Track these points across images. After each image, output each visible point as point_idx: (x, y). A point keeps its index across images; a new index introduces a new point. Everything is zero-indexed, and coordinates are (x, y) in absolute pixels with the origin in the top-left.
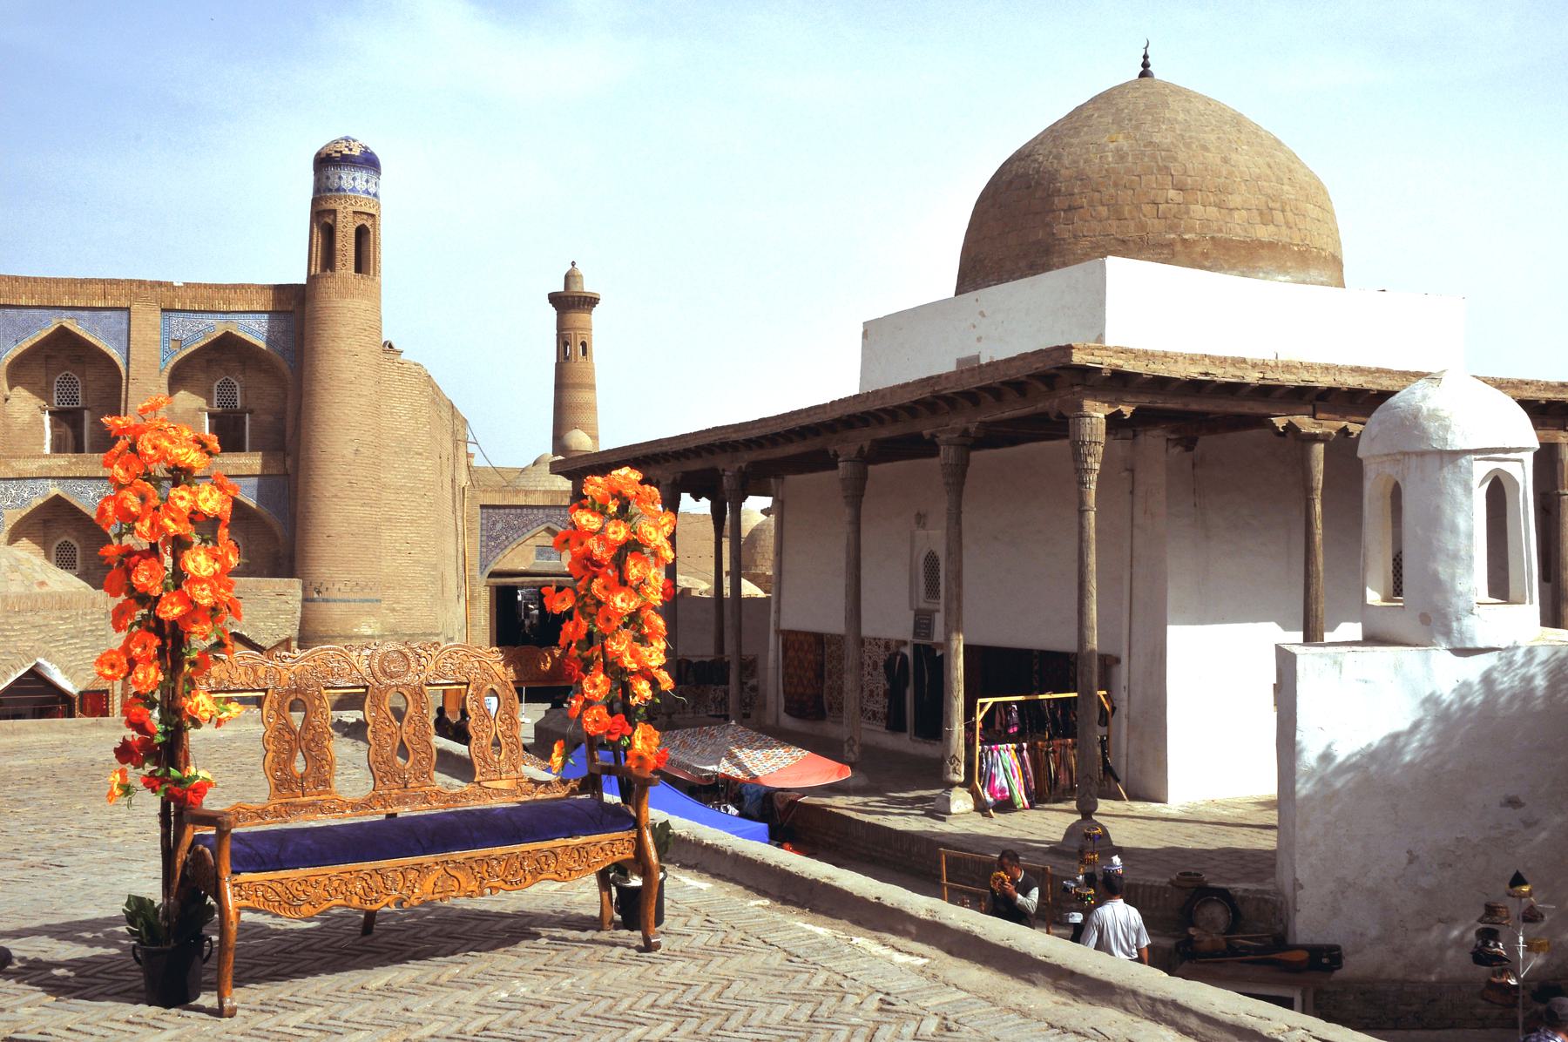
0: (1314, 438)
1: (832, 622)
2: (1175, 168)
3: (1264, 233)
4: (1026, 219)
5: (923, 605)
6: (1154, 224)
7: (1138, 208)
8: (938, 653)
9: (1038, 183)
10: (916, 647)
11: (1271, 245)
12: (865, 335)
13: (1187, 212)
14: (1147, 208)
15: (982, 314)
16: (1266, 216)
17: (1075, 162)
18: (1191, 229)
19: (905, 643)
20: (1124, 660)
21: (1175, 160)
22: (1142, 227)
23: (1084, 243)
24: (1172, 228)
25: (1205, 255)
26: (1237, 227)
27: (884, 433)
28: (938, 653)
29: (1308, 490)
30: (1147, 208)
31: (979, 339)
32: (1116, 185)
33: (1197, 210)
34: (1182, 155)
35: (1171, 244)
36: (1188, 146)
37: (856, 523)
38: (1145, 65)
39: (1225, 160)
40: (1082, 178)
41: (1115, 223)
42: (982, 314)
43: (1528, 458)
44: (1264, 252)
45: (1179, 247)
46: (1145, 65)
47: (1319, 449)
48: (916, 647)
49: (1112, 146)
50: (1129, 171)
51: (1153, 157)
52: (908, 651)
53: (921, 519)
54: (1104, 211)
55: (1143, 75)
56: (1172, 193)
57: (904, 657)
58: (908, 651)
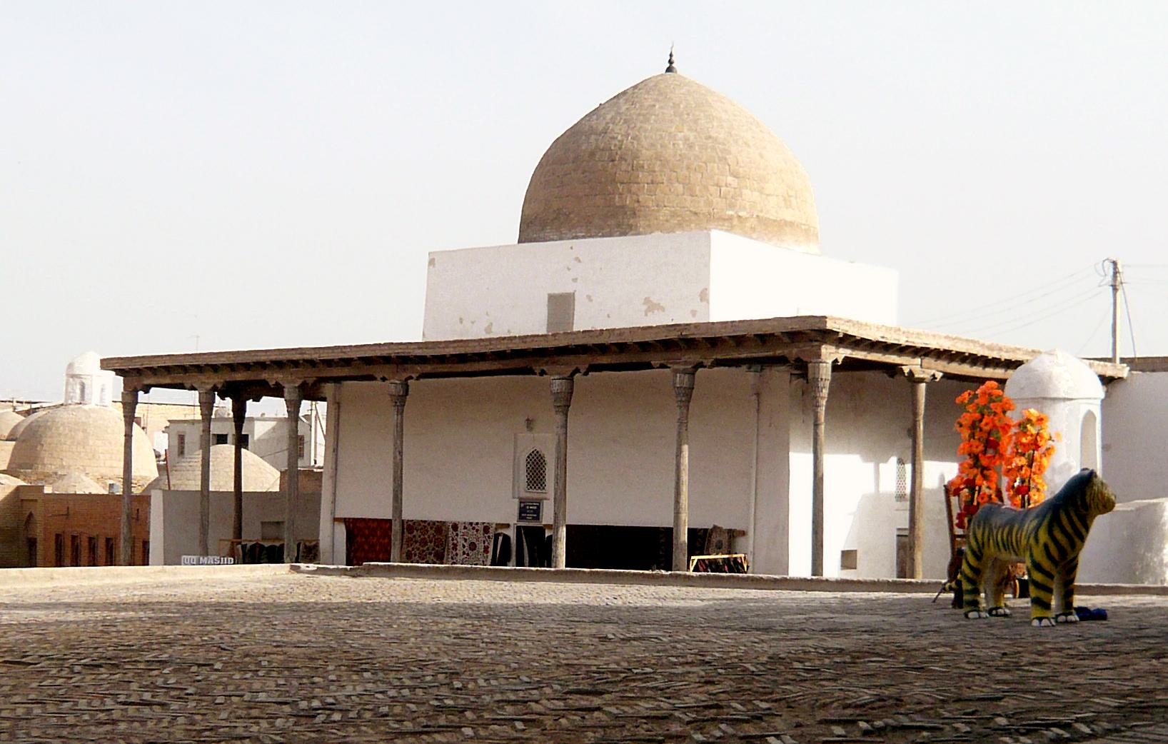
0: (922, 380)
1: (382, 511)
2: (730, 159)
3: (787, 215)
4: (585, 185)
5: (524, 495)
6: (719, 203)
7: (706, 188)
8: (547, 534)
9: (622, 158)
10: (518, 528)
11: (791, 224)
12: (432, 262)
13: (741, 195)
14: (712, 189)
15: (578, 260)
16: (787, 201)
17: (652, 145)
18: (744, 209)
19: (508, 526)
20: (751, 533)
21: (730, 153)
22: (709, 203)
23: (666, 211)
24: (731, 206)
25: (753, 229)
26: (774, 210)
27: (860, 355)
28: (547, 534)
29: (915, 414)
30: (712, 189)
31: (575, 280)
32: (688, 168)
33: (746, 192)
34: (734, 149)
35: (730, 219)
36: (736, 141)
37: (1054, 399)
38: (671, 62)
39: (761, 156)
40: (658, 157)
41: (689, 198)
42: (578, 260)
43: (1099, 402)
44: (788, 229)
45: (735, 222)
46: (671, 62)
47: (923, 385)
48: (518, 528)
49: (680, 135)
50: (697, 157)
51: (713, 148)
52: (511, 533)
53: (530, 423)
54: (680, 188)
55: (669, 70)
56: (730, 179)
57: (506, 538)
58: (511, 533)
